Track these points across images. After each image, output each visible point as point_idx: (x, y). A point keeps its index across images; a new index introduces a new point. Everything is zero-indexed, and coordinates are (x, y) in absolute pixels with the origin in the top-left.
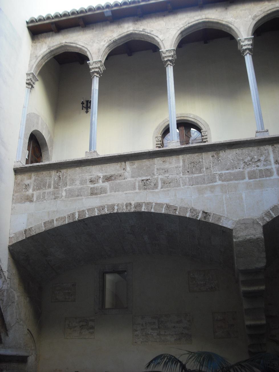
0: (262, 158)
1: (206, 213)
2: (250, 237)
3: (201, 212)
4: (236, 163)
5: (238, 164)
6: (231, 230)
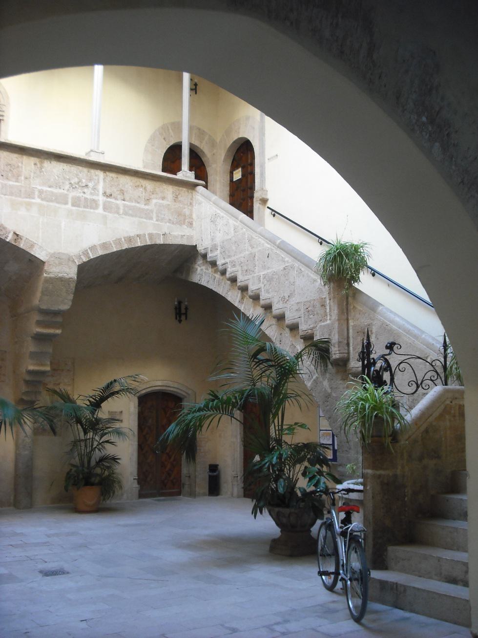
0: (91, 185)
1: (17, 235)
2: (63, 276)
3: (12, 233)
4: (61, 181)
5: (63, 183)
6: (43, 263)
